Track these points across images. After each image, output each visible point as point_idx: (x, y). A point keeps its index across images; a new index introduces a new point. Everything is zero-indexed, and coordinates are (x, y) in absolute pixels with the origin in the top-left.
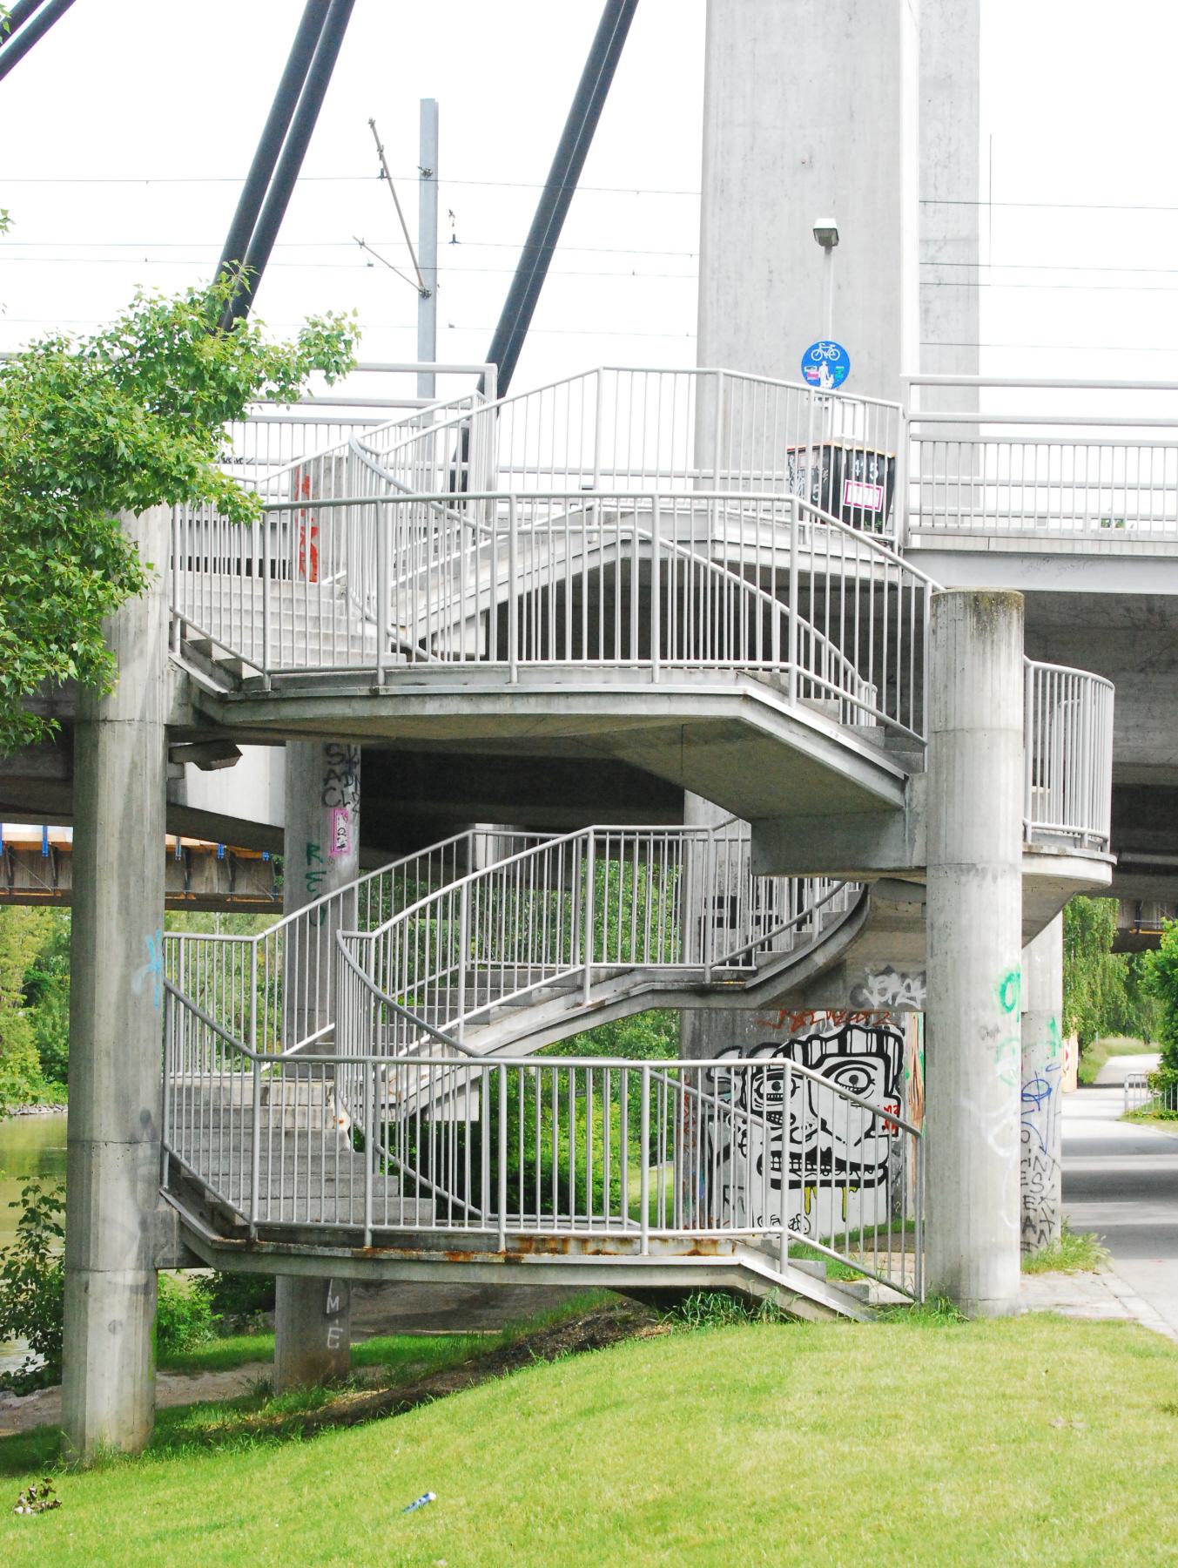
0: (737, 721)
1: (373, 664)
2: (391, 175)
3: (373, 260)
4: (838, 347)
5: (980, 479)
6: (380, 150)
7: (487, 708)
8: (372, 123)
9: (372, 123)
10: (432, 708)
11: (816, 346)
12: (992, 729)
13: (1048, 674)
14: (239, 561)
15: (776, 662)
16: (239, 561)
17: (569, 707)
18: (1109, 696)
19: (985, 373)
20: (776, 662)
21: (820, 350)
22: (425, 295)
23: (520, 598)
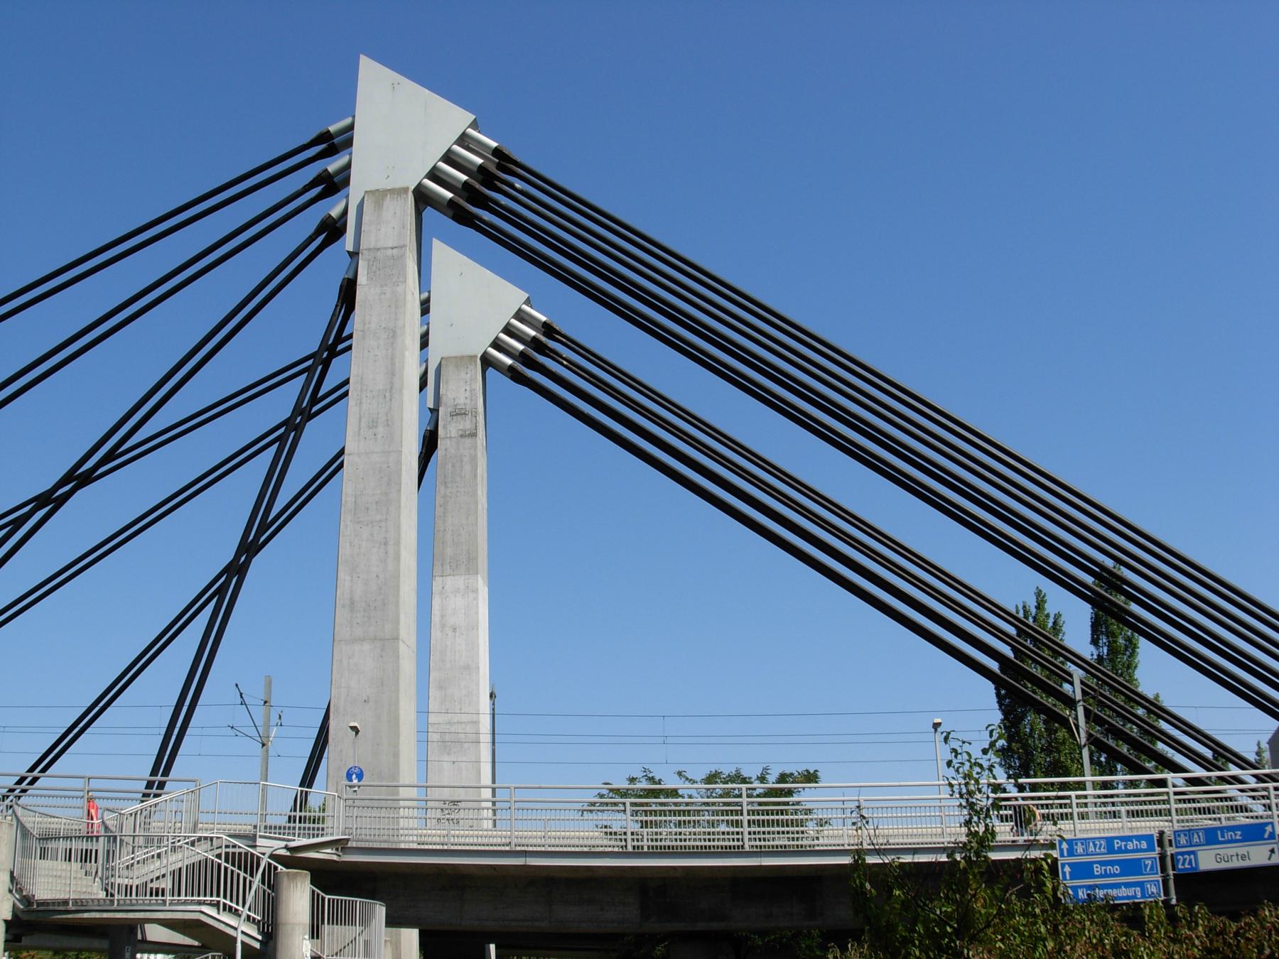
0: (198, 921)
1: (67, 897)
2: (247, 703)
3: (238, 733)
4: (359, 768)
5: (481, 817)
6: (241, 694)
7: (105, 915)
8: (237, 685)
9: (237, 685)
10: (86, 915)
11: (351, 768)
12: (293, 924)
13: (336, 901)
14: (82, 850)
15: (128, 897)
16: (82, 850)
17: (134, 915)
18: (384, 909)
19: (401, 783)
20: (128, 897)
21: (353, 769)
22: (263, 745)
23: (187, 866)
